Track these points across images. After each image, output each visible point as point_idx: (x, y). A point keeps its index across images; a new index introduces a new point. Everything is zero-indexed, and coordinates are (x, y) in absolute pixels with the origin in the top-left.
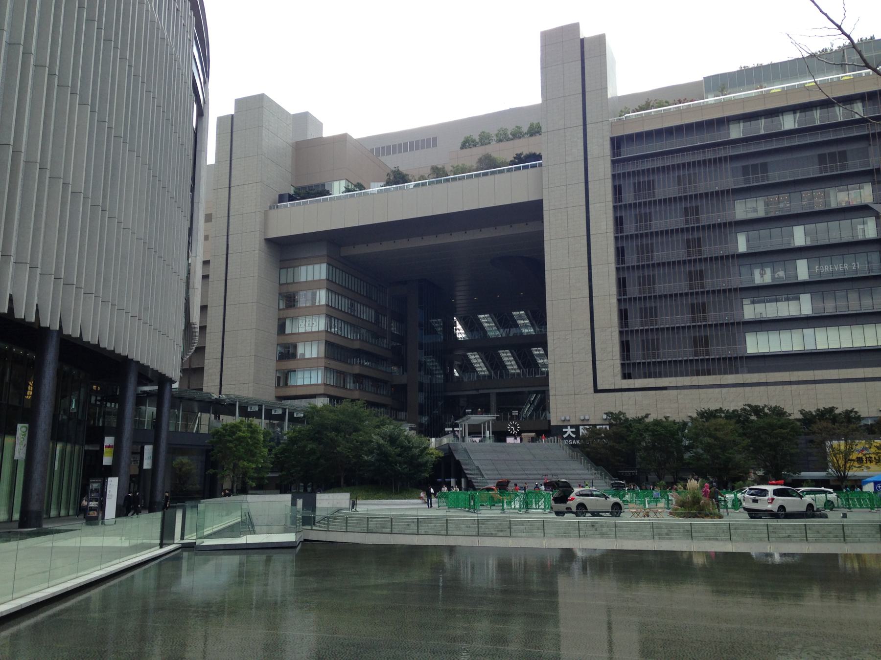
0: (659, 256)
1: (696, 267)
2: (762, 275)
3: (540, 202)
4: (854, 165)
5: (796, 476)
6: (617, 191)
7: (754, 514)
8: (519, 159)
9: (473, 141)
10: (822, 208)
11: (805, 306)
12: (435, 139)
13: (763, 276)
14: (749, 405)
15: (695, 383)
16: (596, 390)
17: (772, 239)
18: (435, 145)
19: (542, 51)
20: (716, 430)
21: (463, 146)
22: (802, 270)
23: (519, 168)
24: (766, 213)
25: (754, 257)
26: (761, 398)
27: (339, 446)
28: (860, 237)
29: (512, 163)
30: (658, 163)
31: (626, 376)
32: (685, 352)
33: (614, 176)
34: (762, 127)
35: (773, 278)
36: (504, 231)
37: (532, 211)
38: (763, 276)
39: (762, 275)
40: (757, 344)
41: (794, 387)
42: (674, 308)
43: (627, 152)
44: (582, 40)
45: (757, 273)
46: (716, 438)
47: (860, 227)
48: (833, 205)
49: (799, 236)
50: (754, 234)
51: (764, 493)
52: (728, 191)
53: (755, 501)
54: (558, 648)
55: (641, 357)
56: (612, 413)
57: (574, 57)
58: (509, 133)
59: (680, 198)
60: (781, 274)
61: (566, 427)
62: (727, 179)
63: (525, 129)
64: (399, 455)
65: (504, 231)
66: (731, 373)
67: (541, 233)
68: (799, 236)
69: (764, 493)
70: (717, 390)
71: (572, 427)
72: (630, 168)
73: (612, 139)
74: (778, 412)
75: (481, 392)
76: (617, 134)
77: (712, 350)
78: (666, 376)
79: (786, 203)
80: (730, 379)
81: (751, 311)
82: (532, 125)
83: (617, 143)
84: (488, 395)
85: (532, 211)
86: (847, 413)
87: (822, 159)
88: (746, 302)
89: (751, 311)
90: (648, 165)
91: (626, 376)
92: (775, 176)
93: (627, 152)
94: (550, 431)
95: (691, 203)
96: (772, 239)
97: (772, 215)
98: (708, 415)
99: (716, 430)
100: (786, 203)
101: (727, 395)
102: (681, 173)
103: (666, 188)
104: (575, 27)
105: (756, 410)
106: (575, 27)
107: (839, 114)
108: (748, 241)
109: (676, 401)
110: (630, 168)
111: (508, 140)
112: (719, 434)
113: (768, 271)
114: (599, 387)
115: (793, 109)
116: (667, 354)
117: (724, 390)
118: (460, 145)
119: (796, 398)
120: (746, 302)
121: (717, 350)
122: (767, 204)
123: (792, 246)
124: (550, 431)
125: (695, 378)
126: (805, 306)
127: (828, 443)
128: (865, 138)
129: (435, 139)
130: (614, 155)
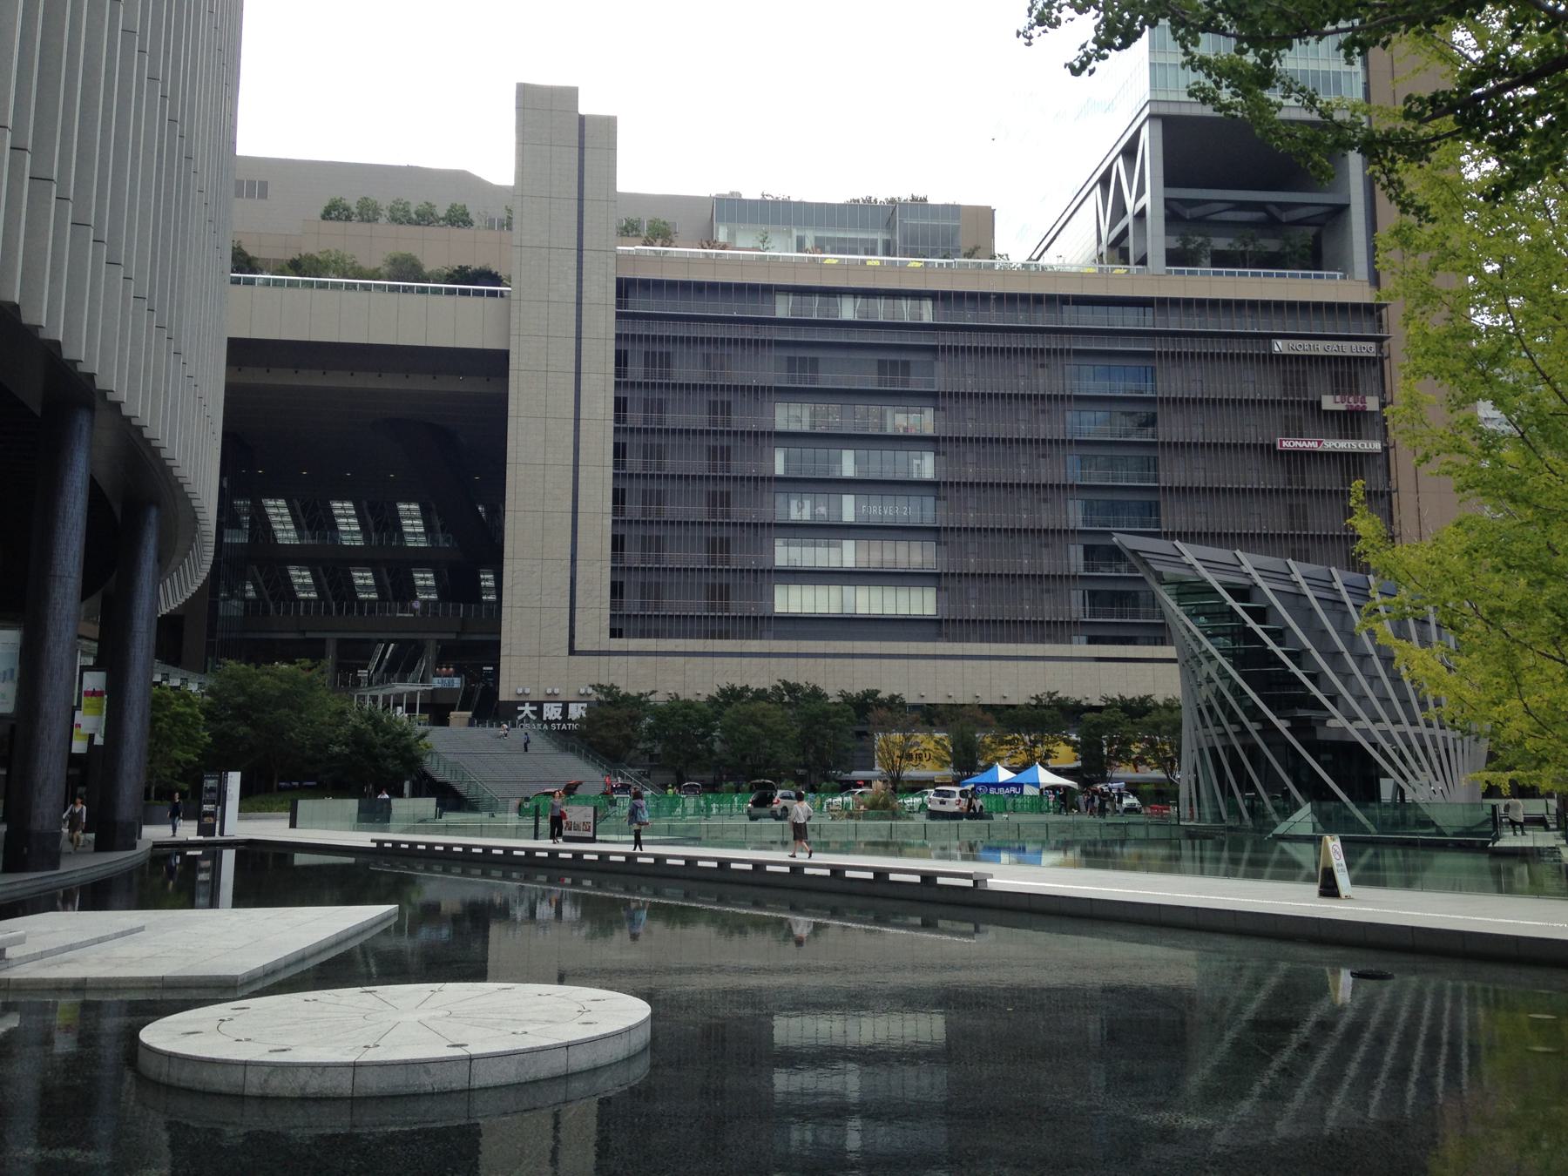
0: (672, 464)
1: (721, 488)
2: (801, 509)
3: (505, 355)
4: (917, 383)
5: (846, 776)
6: (621, 359)
7: (934, 815)
8: (462, 275)
9: (346, 209)
10: (877, 432)
11: (848, 555)
12: (264, 186)
13: (800, 510)
14: (785, 683)
15: (653, 649)
16: (572, 652)
17: (813, 461)
18: (263, 195)
19: (518, 114)
20: (764, 716)
21: (327, 215)
22: (848, 509)
23: (464, 293)
24: (813, 425)
25: (795, 483)
26: (803, 673)
27: (293, 730)
28: (915, 476)
29: (450, 279)
30: (681, 330)
31: (615, 633)
32: (696, 605)
33: (618, 337)
34: (815, 309)
35: (813, 515)
36: (422, 384)
37: (495, 364)
38: (800, 510)
39: (801, 509)
40: (791, 600)
41: (829, 661)
42: (687, 541)
43: (639, 304)
44: (582, 119)
45: (794, 504)
46: (761, 725)
47: (916, 462)
48: (889, 431)
49: (848, 464)
50: (795, 451)
51: (949, 794)
52: (770, 388)
53: (943, 803)
54: (1456, 804)
55: (636, 611)
56: (601, 686)
57: (562, 132)
58: (412, 210)
59: (709, 386)
60: (822, 510)
61: (523, 704)
62: (767, 370)
63: (441, 212)
64: (387, 747)
65: (422, 384)
66: (755, 638)
67: (502, 402)
68: (848, 464)
69: (949, 794)
70: (736, 660)
71: (532, 703)
72: (641, 329)
73: (619, 281)
74: (816, 694)
75: (309, 635)
76: (628, 275)
77: (732, 608)
78: (671, 636)
79: (835, 417)
80: (754, 645)
81: (785, 554)
82: (453, 207)
83: (625, 288)
84: (323, 641)
85: (495, 364)
86: (893, 698)
87: (882, 365)
88: (778, 542)
89: (785, 554)
90: (668, 330)
91: (615, 633)
92: (826, 379)
93: (639, 304)
94: (507, 713)
95: (721, 397)
96: (813, 461)
97: (818, 430)
98: (732, 695)
99: (764, 716)
100: (835, 417)
101: (753, 667)
102: (712, 350)
103: (687, 369)
104: (571, 94)
105: (792, 689)
106: (571, 94)
107: (905, 311)
108: (787, 460)
109: (682, 672)
110: (641, 329)
111: (410, 222)
112: (768, 722)
113: (807, 504)
114: (577, 647)
115: (855, 293)
116: (674, 604)
117: (745, 660)
118: (321, 211)
119: (839, 675)
120: (778, 542)
121: (739, 606)
122: (814, 415)
123: (837, 475)
124: (507, 713)
125: (709, 641)
126: (848, 555)
127: (879, 737)
128: (934, 349)
129: (264, 186)
130: (619, 305)
